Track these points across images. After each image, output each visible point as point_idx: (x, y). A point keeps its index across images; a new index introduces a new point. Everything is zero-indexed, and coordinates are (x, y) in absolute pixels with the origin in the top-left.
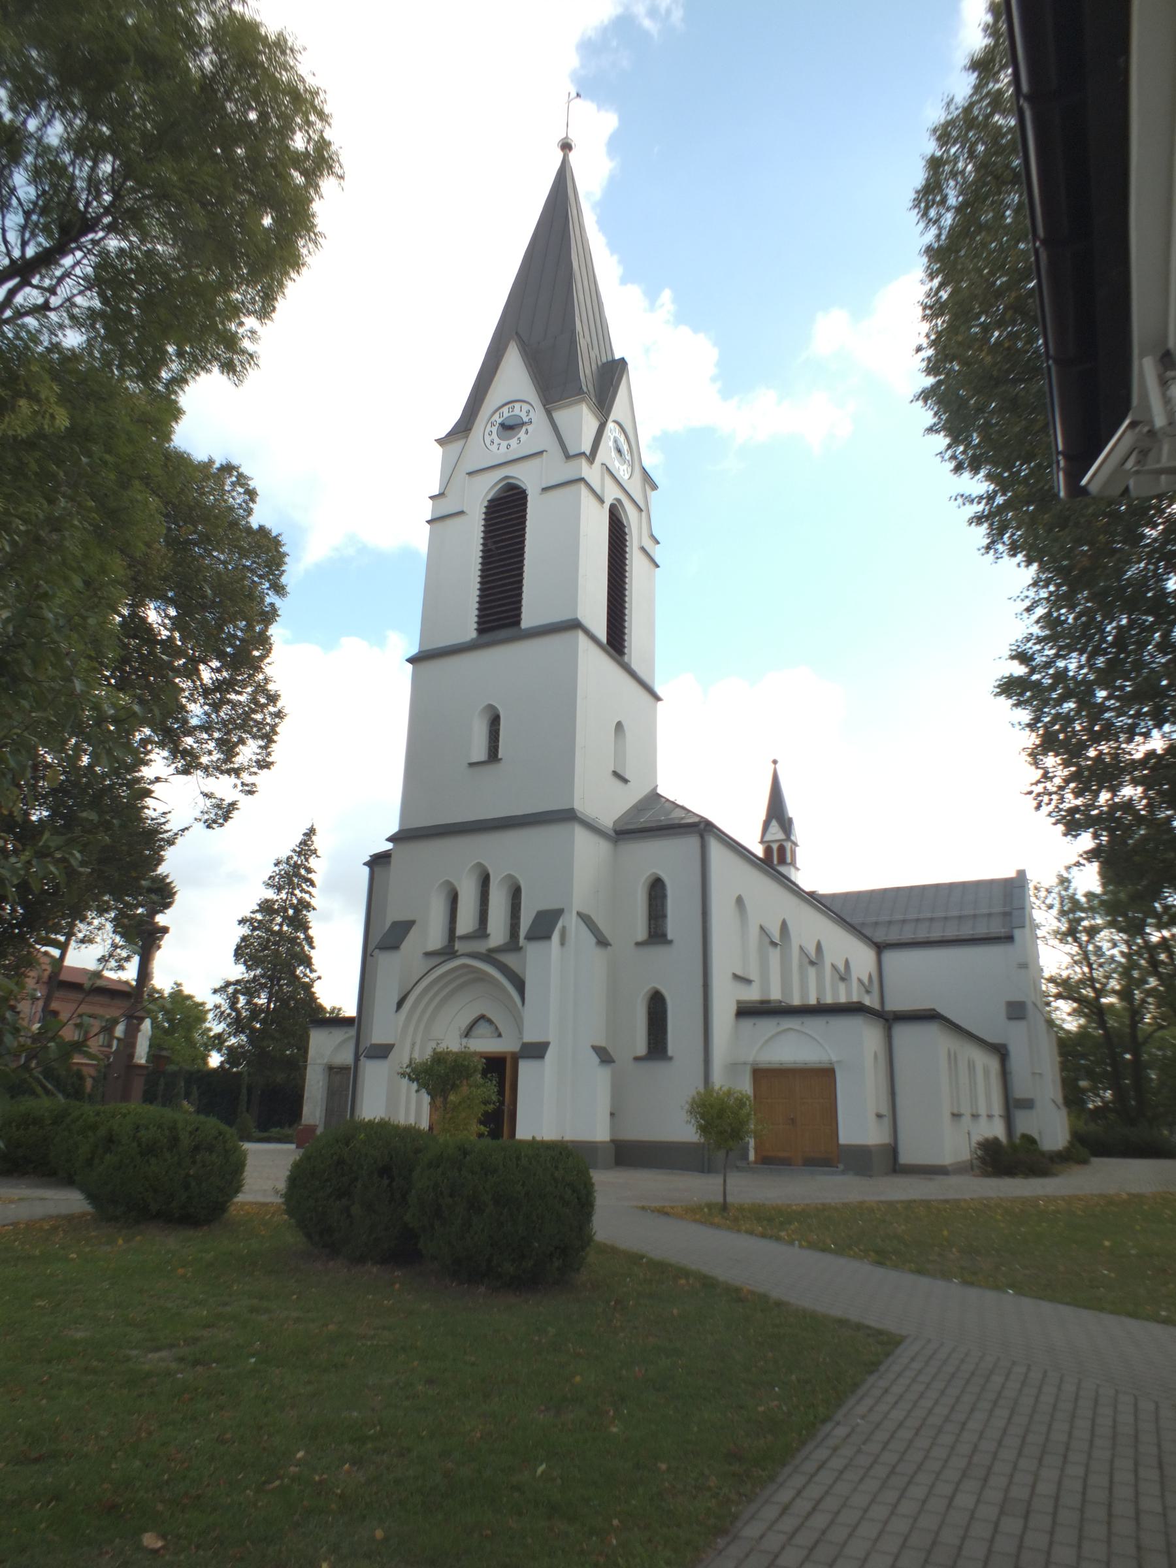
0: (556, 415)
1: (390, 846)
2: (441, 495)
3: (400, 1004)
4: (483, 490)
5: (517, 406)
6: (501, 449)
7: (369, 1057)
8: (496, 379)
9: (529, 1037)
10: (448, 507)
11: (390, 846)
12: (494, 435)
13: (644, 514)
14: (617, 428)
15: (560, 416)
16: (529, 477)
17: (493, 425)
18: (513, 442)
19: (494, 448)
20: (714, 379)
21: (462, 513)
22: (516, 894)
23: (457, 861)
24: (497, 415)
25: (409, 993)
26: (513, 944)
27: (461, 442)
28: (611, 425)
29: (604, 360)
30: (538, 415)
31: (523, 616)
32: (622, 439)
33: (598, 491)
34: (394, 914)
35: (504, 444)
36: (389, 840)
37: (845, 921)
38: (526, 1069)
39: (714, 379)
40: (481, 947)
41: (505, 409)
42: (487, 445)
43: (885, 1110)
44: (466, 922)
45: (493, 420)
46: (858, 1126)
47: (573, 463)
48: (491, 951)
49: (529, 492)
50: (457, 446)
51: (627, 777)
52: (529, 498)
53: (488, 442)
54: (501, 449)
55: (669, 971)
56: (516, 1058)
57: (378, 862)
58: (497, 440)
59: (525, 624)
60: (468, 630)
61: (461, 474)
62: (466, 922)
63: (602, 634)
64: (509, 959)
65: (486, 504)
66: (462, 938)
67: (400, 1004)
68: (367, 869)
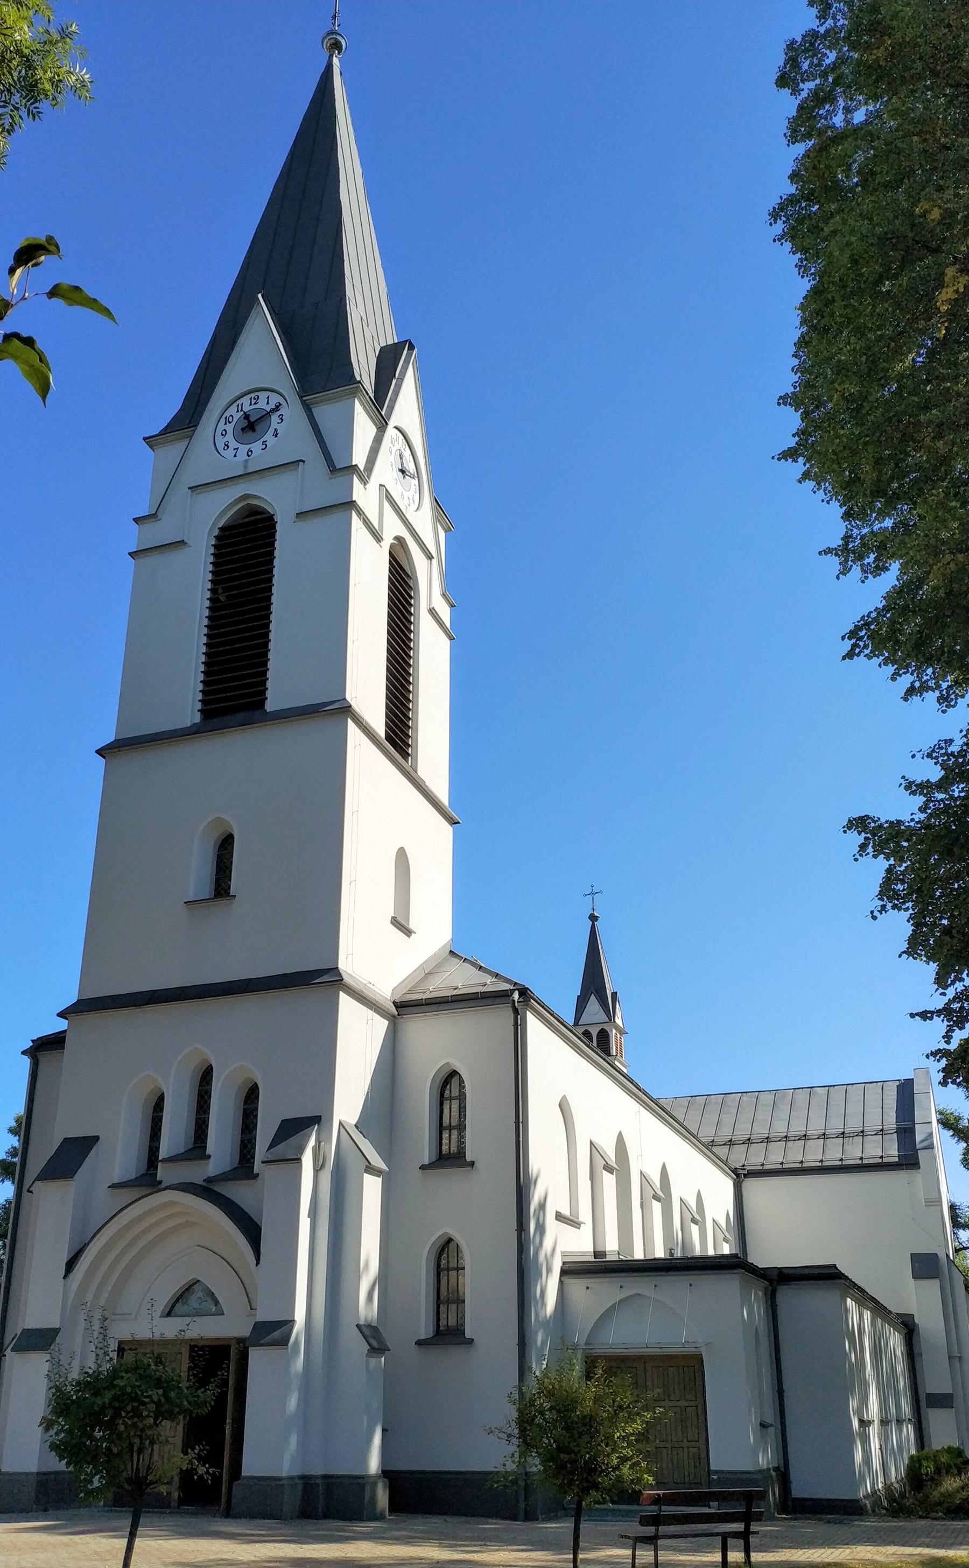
0: (317, 411)
1: (62, 1025)
2: (153, 517)
3: (70, 1265)
4: (215, 510)
5: (263, 395)
6: (236, 456)
7: (18, 1349)
8: (234, 355)
9: (263, 1315)
10: (161, 533)
11: (62, 1025)
12: (230, 437)
13: (435, 561)
14: (401, 437)
15: (325, 413)
16: (278, 497)
17: (227, 421)
18: (257, 447)
19: (231, 452)
20: (33, 1041)
21: (182, 543)
22: (252, 1095)
23: (161, 1054)
24: (234, 407)
25: (86, 1245)
26: (244, 1166)
27: (182, 445)
28: (391, 432)
29: (383, 344)
30: (293, 411)
31: (269, 694)
32: (407, 453)
33: (386, 505)
34: (64, 1125)
35: (244, 449)
36: (61, 1015)
37: (915, 1376)
38: (257, 1358)
39: (33, 1041)
40: (197, 1173)
41: (245, 401)
42: (216, 448)
43: (770, 1416)
44: (174, 1136)
45: (227, 414)
46: (736, 1443)
47: (340, 480)
48: (209, 1180)
49: (278, 518)
50: (173, 451)
51: (412, 926)
52: (278, 527)
53: (220, 446)
54: (236, 456)
55: (464, 1209)
56: (243, 1346)
57: (45, 1048)
58: (233, 444)
59: (270, 706)
60: (188, 710)
61: (181, 489)
62: (174, 1136)
63: (379, 725)
64: (239, 1192)
65: (216, 532)
66: (164, 1161)
67: (70, 1265)
68: (26, 1061)
